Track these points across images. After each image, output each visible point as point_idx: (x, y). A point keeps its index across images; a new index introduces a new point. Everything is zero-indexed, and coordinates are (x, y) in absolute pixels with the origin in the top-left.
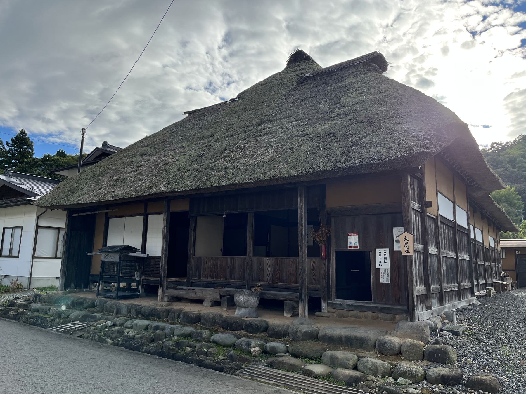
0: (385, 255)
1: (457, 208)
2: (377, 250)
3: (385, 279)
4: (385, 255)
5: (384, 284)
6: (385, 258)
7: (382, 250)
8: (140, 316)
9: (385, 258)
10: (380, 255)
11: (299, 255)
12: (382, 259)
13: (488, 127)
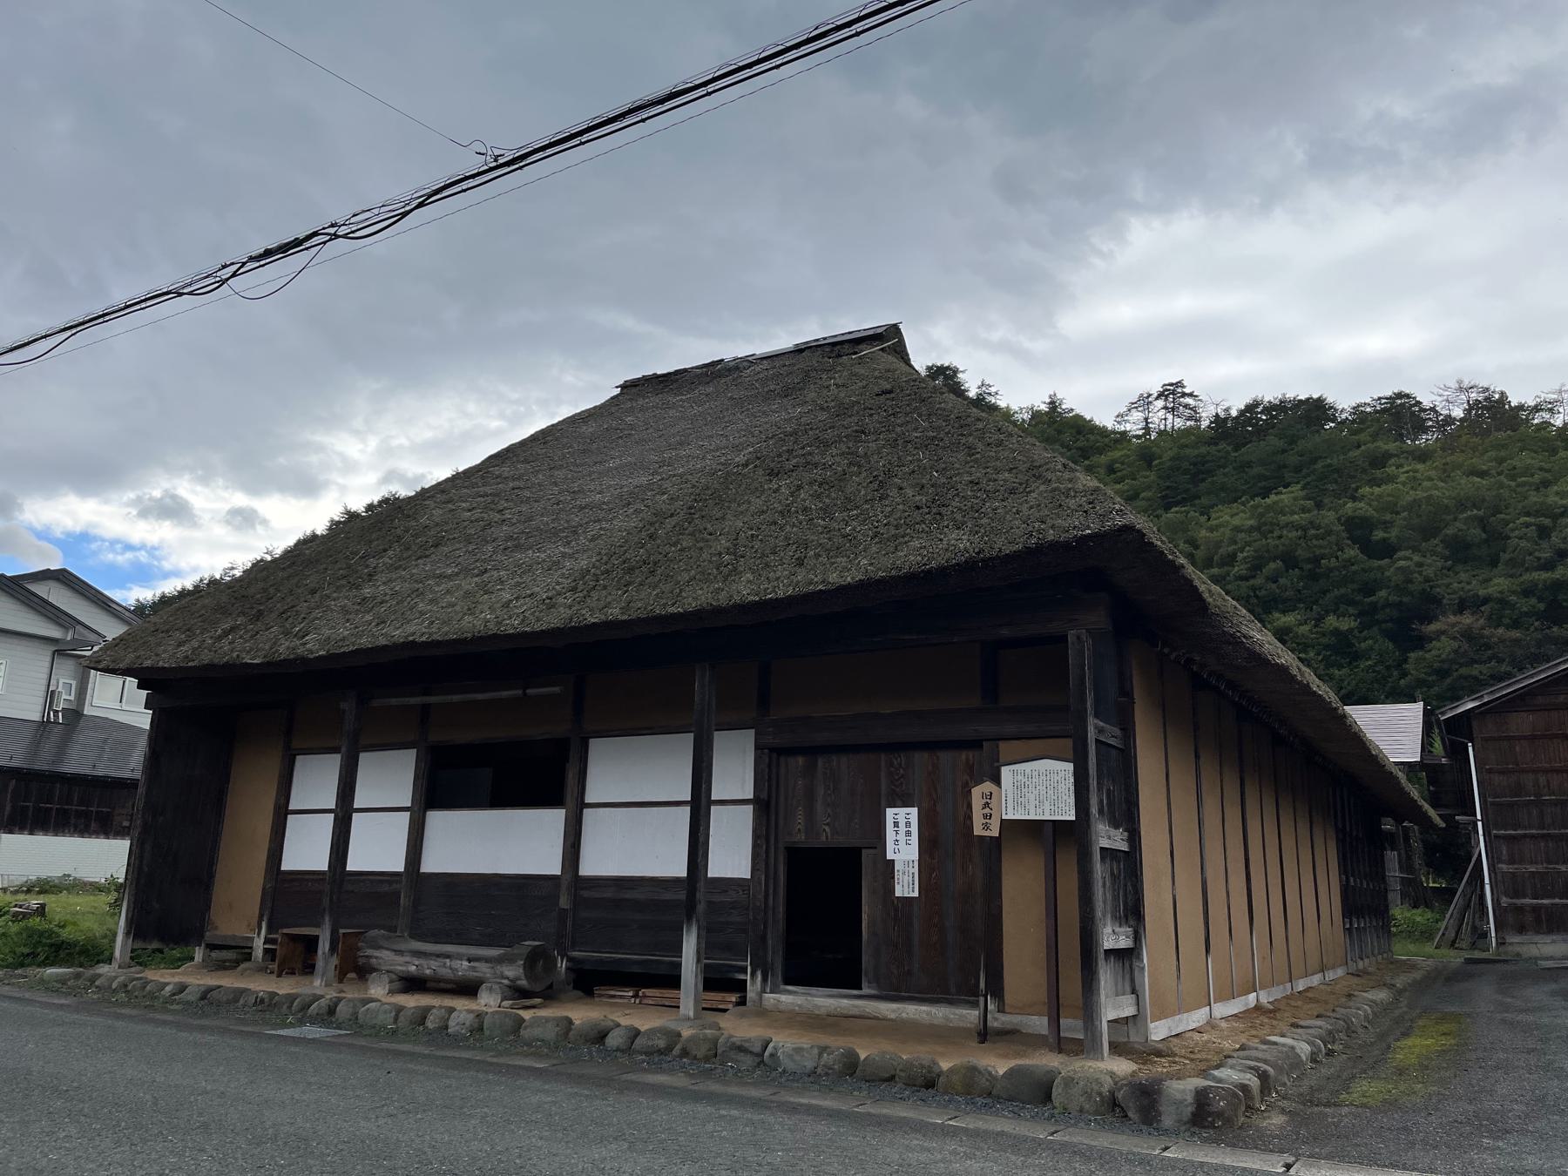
0: (908, 824)
1: (1315, 830)
2: (890, 812)
3: (906, 885)
4: (908, 824)
5: (906, 804)
6: (908, 833)
7: (902, 811)
8: (1277, 1120)
9: (908, 833)
10: (896, 824)
11: (781, 859)
12: (902, 837)
13: (1207, 951)
